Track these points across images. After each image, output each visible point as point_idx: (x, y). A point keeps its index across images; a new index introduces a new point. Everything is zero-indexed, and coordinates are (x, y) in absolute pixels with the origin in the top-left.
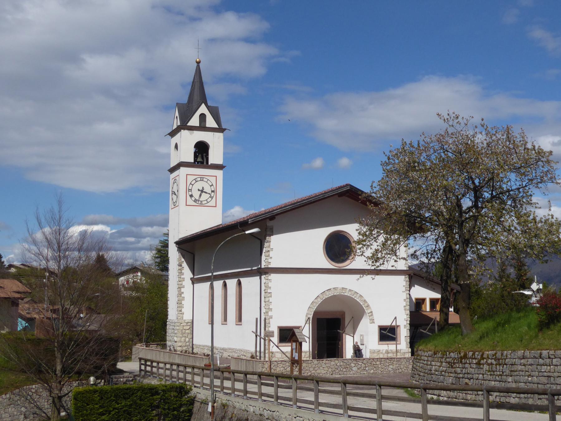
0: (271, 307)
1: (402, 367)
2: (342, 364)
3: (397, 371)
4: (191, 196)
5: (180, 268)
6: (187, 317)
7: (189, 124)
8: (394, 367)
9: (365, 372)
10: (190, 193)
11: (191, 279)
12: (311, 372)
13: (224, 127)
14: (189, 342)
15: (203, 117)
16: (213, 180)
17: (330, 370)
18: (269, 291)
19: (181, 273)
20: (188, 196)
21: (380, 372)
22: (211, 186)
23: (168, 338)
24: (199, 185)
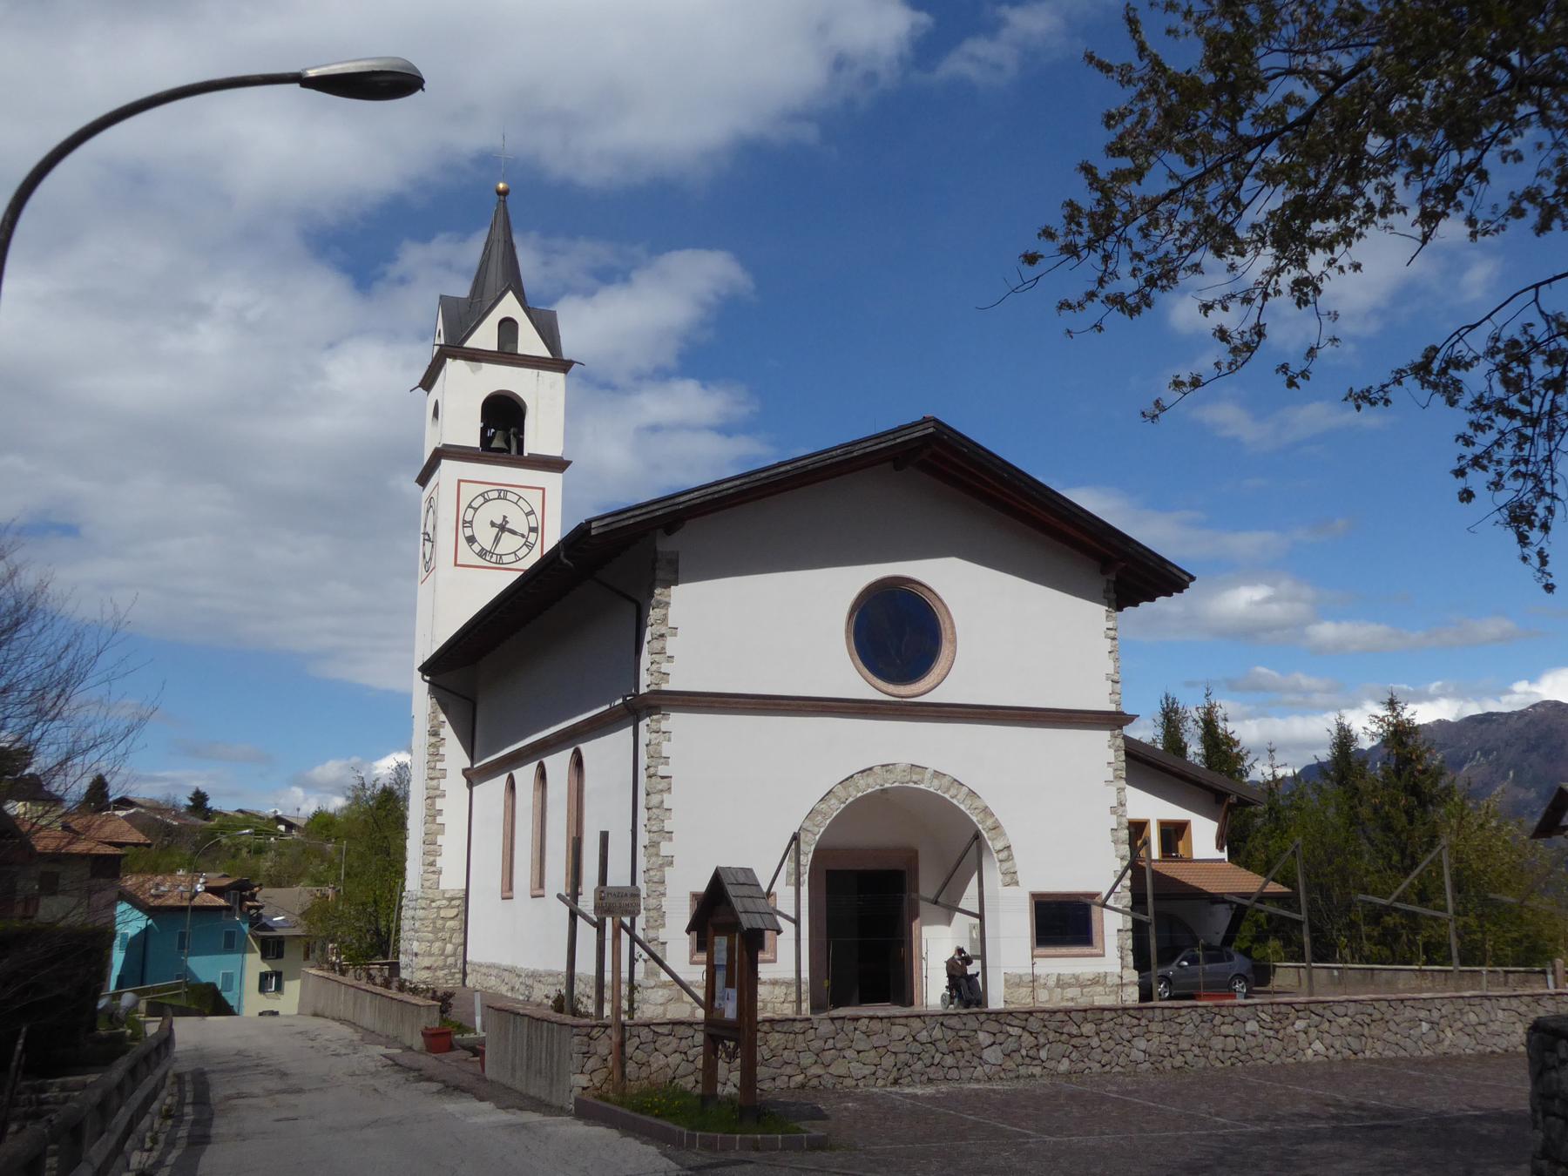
0: (668, 826)
1: (1184, 1046)
2: (937, 1033)
3: (1167, 1063)
4: (471, 540)
5: (433, 740)
6: (451, 881)
7: (468, 344)
8: (1153, 1046)
9: (1037, 1071)
10: (468, 532)
11: (465, 772)
12: (803, 1070)
13: (566, 356)
14: (454, 954)
15: (508, 328)
16: (534, 498)
17: (888, 1061)
18: (662, 770)
19: (435, 754)
20: (462, 542)
21: (1096, 1067)
22: (527, 514)
23: (403, 945)
24: (495, 511)
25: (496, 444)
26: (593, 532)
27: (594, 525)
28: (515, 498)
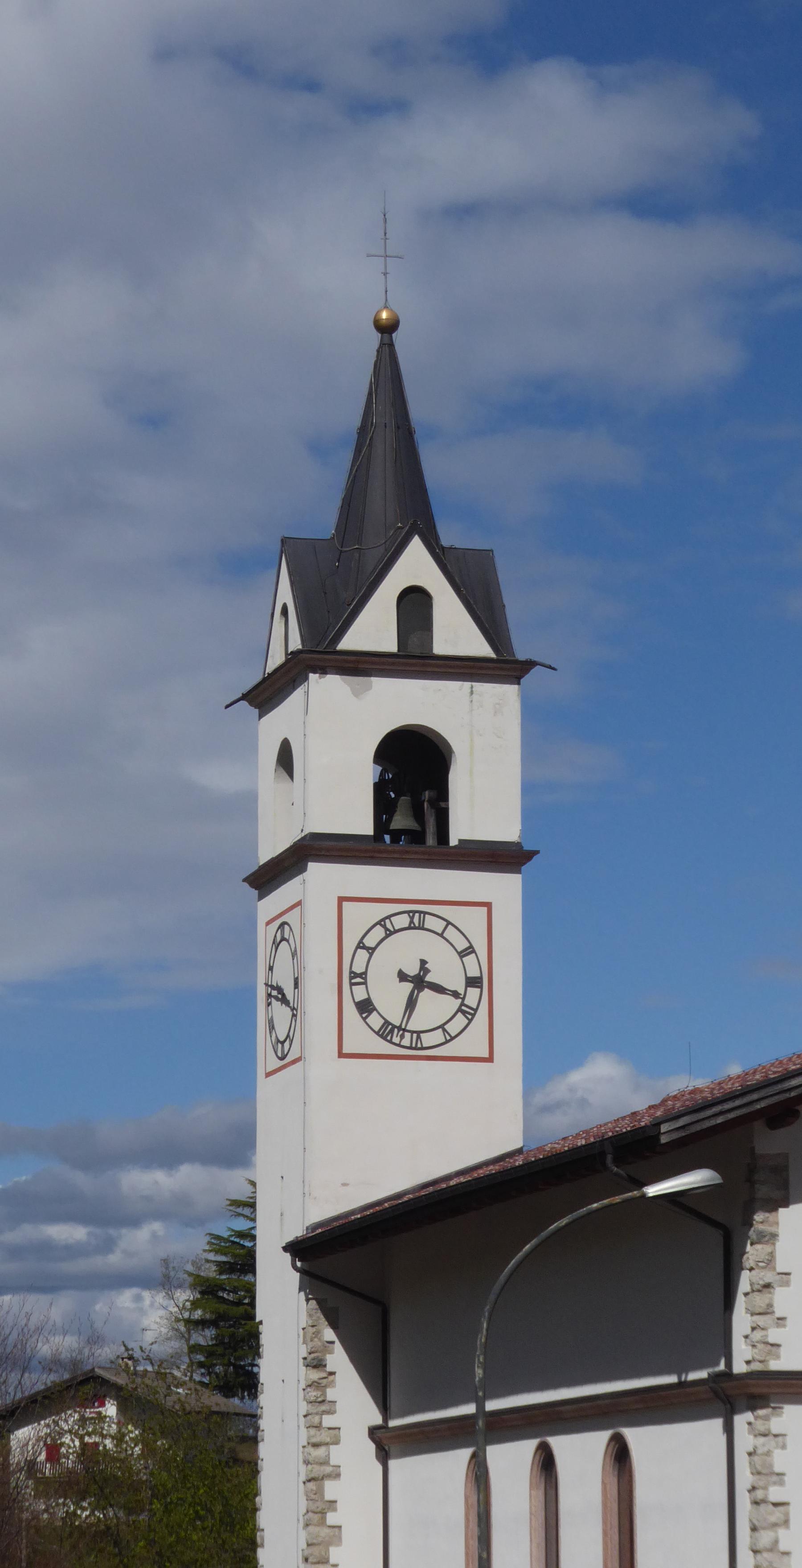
4: (365, 1007)
5: (315, 1375)
10: (360, 993)
11: (373, 1432)
13: (521, 654)
15: (415, 604)
19: (319, 1400)
20: (351, 1012)
22: (462, 954)
25: (400, 821)
26: (664, 1140)
27: (664, 1128)
28: (438, 926)
